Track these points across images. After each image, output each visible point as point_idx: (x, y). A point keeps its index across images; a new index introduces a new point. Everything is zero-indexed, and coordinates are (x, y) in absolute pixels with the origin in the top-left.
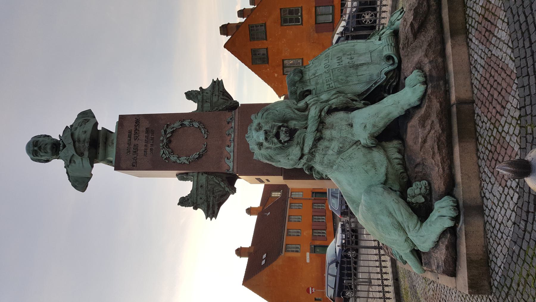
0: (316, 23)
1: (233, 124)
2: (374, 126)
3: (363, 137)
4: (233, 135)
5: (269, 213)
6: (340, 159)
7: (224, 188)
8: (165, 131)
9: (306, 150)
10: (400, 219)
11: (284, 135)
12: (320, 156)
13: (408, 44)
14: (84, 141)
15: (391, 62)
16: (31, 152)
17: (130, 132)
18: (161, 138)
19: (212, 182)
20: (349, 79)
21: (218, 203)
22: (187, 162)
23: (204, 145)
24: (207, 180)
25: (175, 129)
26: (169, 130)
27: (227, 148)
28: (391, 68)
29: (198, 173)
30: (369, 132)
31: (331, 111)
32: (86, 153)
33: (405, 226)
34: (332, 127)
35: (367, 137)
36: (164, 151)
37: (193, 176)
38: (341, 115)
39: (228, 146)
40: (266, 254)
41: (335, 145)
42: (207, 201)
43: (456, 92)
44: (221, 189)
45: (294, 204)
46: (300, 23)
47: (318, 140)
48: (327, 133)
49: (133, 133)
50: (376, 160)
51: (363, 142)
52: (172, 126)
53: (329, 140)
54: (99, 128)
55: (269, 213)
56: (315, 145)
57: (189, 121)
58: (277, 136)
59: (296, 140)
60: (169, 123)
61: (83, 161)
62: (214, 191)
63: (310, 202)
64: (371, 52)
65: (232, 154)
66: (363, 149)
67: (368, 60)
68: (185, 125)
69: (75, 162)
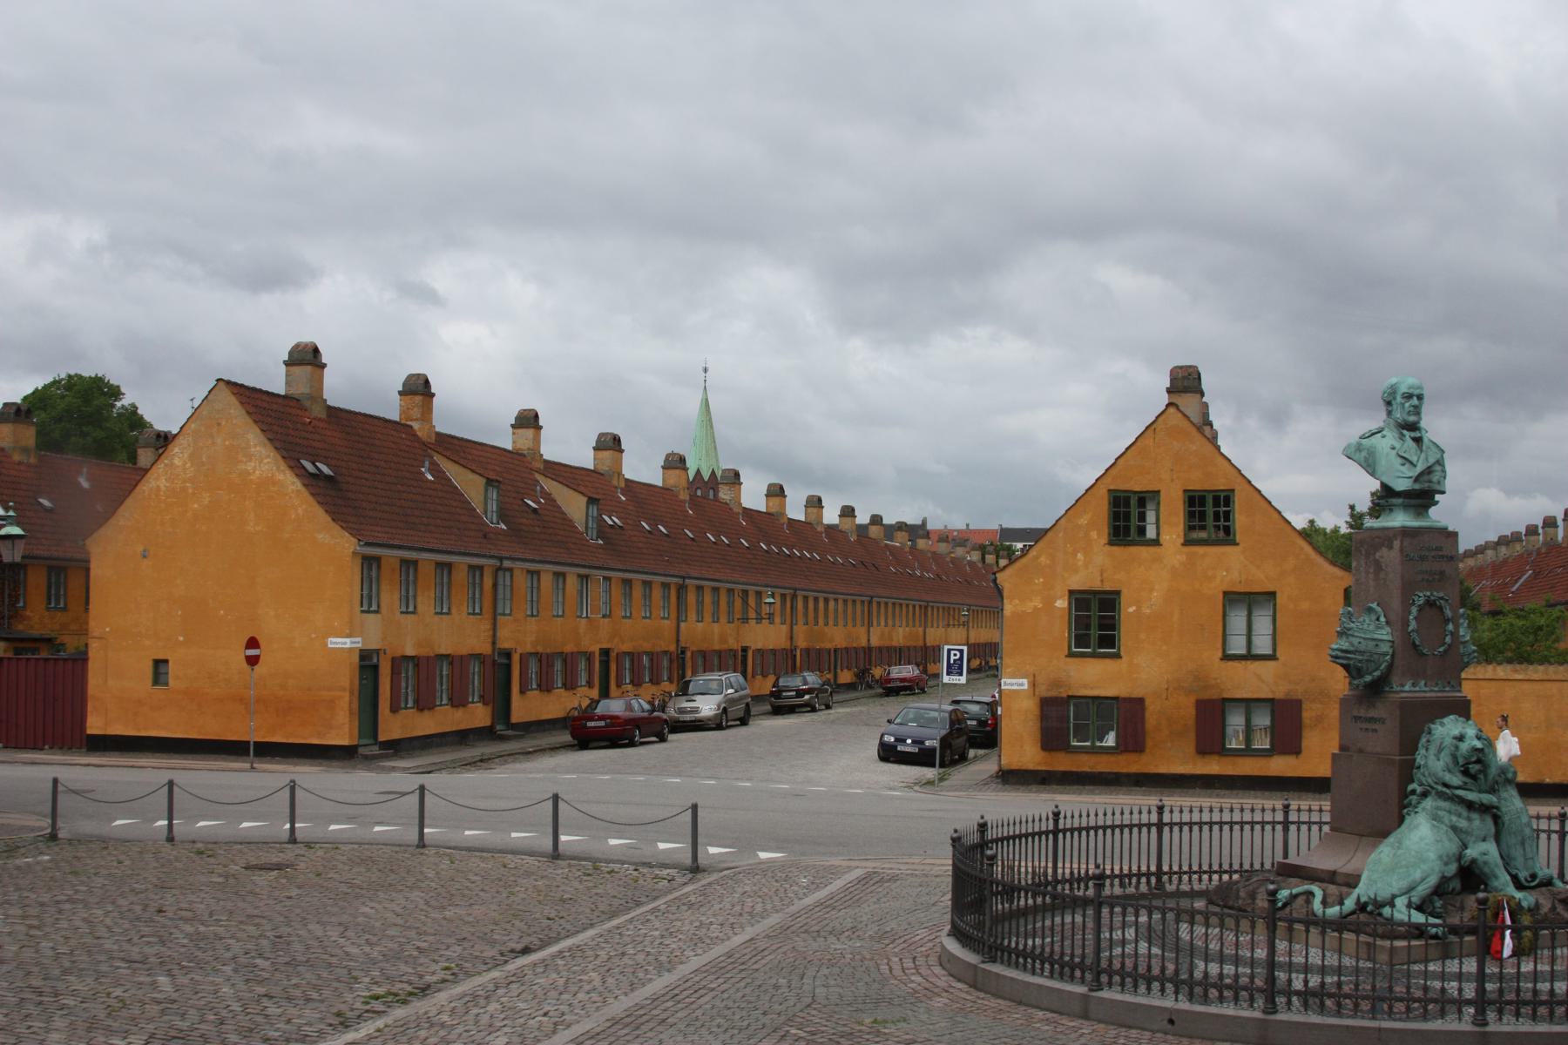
0: (1225, 700)
2: (1485, 863)
3: (1471, 852)
4: (1436, 689)
5: (430, 477)
6: (1445, 828)
7: (1370, 674)
8: (1442, 598)
9: (1459, 792)
10: (1420, 888)
14: (1430, 482)
16: (1411, 391)
17: (1440, 549)
18: (1435, 593)
19: (1381, 659)
22: (1410, 628)
24: (1385, 654)
27: (1423, 682)
28: (1523, 879)
29: (1393, 642)
31: (1497, 819)
32: (1417, 486)
34: (1483, 820)
38: (1493, 830)
39: (1426, 685)
40: (331, 474)
41: (1463, 824)
44: (1370, 670)
45: (445, 580)
47: (1470, 806)
48: (1475, 816)
49: (1440, 553)
50: (1450, 866)
51: (1468, 852)
54: (1437, 497)
55: (430, 477)
58: (1478, 761)
63: (486, 649)
65: (1417, 689)
69: (1403, 465)
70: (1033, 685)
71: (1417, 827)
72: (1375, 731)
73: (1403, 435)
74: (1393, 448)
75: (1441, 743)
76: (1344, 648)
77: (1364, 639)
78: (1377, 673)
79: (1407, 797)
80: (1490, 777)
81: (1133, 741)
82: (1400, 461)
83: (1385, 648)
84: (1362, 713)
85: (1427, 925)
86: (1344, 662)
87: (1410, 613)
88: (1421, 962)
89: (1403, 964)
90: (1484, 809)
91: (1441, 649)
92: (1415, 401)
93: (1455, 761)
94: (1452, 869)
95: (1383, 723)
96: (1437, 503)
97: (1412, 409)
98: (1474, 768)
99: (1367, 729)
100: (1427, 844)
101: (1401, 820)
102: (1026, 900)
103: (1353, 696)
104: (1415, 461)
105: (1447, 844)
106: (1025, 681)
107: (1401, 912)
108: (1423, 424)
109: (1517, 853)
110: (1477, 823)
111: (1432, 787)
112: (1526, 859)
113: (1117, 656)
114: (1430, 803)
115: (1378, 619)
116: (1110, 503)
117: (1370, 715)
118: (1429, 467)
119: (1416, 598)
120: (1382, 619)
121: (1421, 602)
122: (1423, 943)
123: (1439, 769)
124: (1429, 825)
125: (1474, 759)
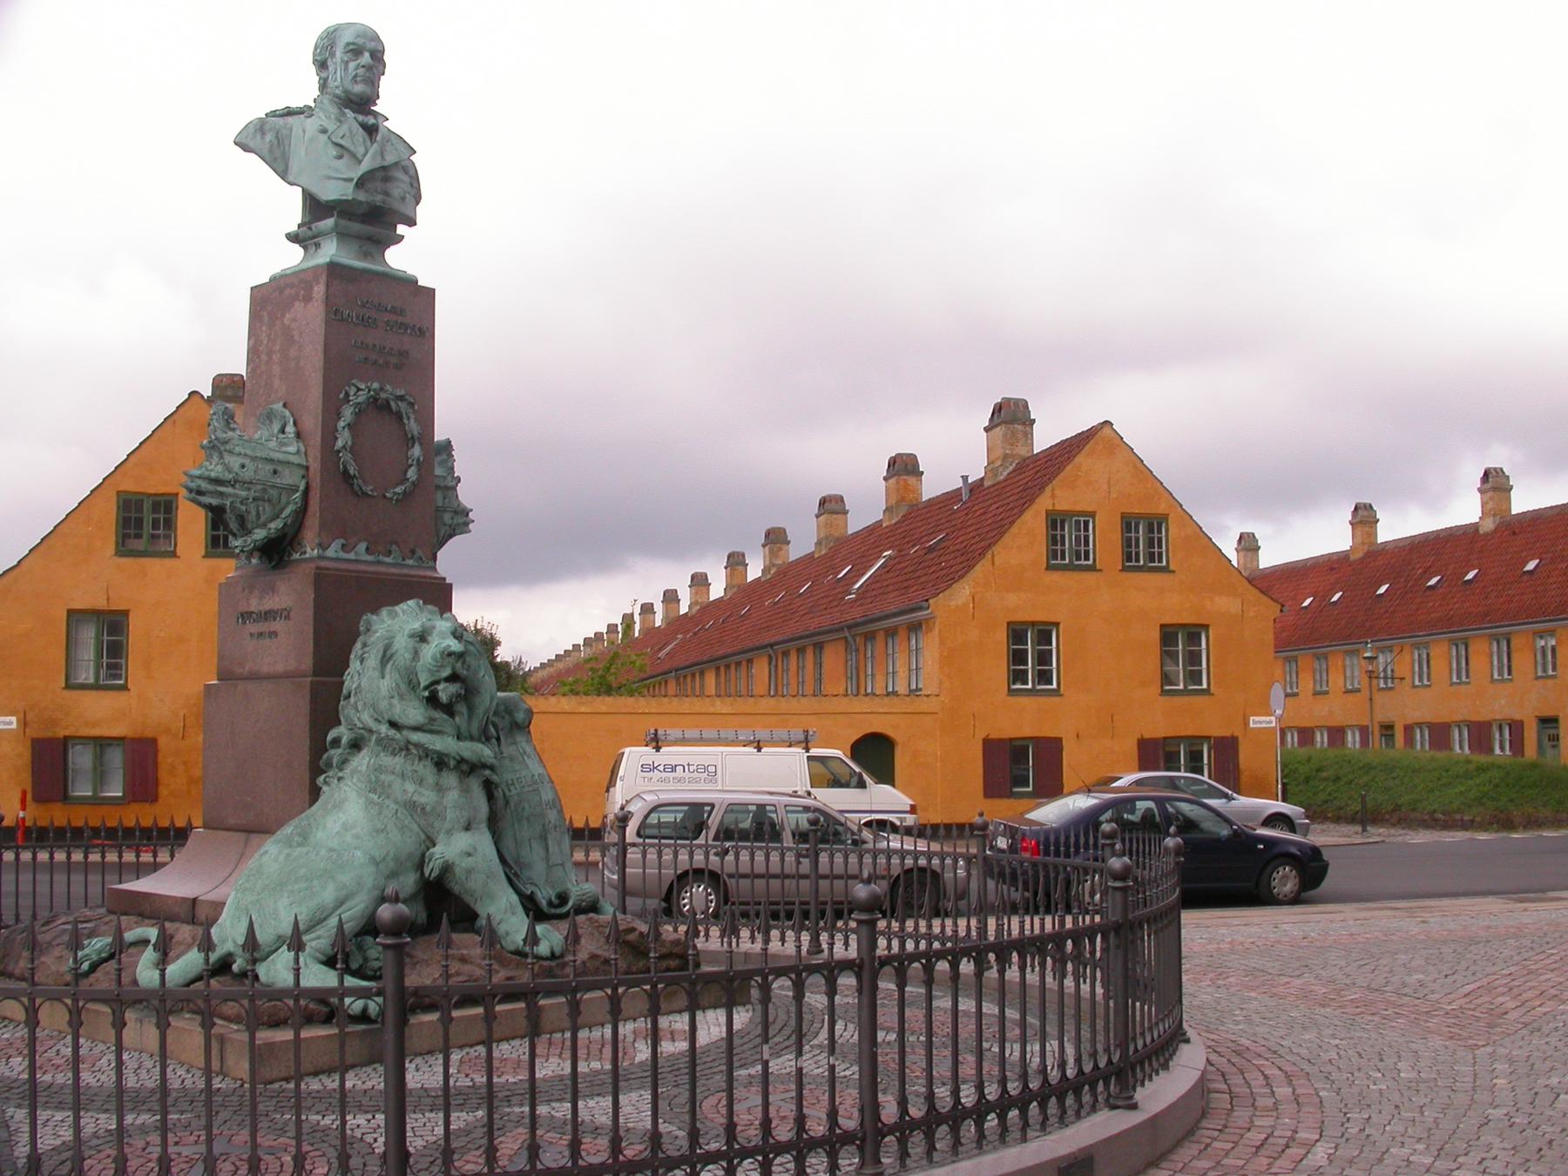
1: (410, 562)
6: (393, 806)
7: (264, 525)
8: (401, 398)
9: (416, 737)
11: (454, 690)
12: (398, 766)
13: (599, 927)
14: (387, 194)
15: (556, 901)
16: (360, 41)
17: (401, 312)
18: (388, 387)
20: (525, 822)
21: (228, 507)
23: (372, 491)
25: (406, 421)
26: (403, 406)
27: (362, 546)
28: (544, 903)
30: (457, 863)
31: (489, 787)
33: (318, 933)
34: (465, 791)
35: (446, 858)
36: (362, 390)
37: (298, 451)
41: (427, 797)
42: (236, 482)
43: (552, 1004)
44: (263, 519)
46: (1031, 789)
47: (440, 763)
49: (400, 319)
52: (412, 416)
53: (437, 784)
54: (401, 229)
56: (427, 756)
57: (421, 459)
58: (453, 678)
59: (438, 715)
60: (416, 407)
61: (341, 182)
62: (260, 503)
64: (562, 865)
65: (352, 556)
66: (418, 853)
67: (555, 859)
68: (413, 447)
69: (340, 157)
70: (24, 723)
71: (339, 806)
72: (273, 634)
73: (344, 114)
74: (324, 131)
75: (387, 647)
76: (213, 475)
77: (254, 459)
78: (276, 525)
79: (326, 750)
80: (480, 711)
81: (143, 785)
82: (333, 152)
83: (289, 477)
84: (254, 605)
85: (343, 992)
86: (214, 501)
87: (339, 416)
88: (329, 1071)
89: (287, 1080)
90: (468, 768)
91: (398, 490)
92: (366, 58)
93: (412, 685)
94: (408, 882)
95: (288, 617)
96: (402, 237)
97: (361, 71)
98: (445, 692)
99: (261, 634)
100: (357, 836)
101: (315, 794)
102: (968, 927)
103: (242, 576)
104: (360, 157)
105: (395, 835)
106: (14, 719)
107: (277, 970)
108: (380, 107)
109: (534, 855)
110: (453, 796)
111: (371, 731)
112: (549, 867)
113: (125, 688)
114: (366, 761)
115: (283, 431)
116: (118, 508)
117: (267, 607)
118: (384, 168)
119: (352, 391)
120: (290, 429)
121: (360, 399)
122: (337, 1031)
123: (384, 691)
124: (362, 801)
125: (446, 673)
